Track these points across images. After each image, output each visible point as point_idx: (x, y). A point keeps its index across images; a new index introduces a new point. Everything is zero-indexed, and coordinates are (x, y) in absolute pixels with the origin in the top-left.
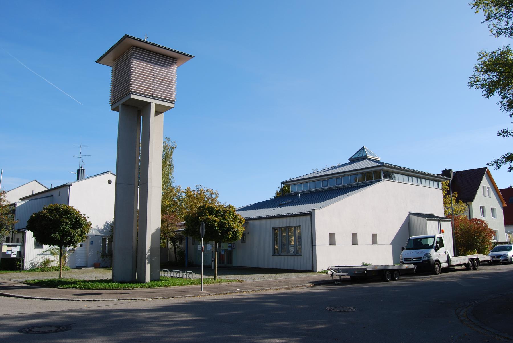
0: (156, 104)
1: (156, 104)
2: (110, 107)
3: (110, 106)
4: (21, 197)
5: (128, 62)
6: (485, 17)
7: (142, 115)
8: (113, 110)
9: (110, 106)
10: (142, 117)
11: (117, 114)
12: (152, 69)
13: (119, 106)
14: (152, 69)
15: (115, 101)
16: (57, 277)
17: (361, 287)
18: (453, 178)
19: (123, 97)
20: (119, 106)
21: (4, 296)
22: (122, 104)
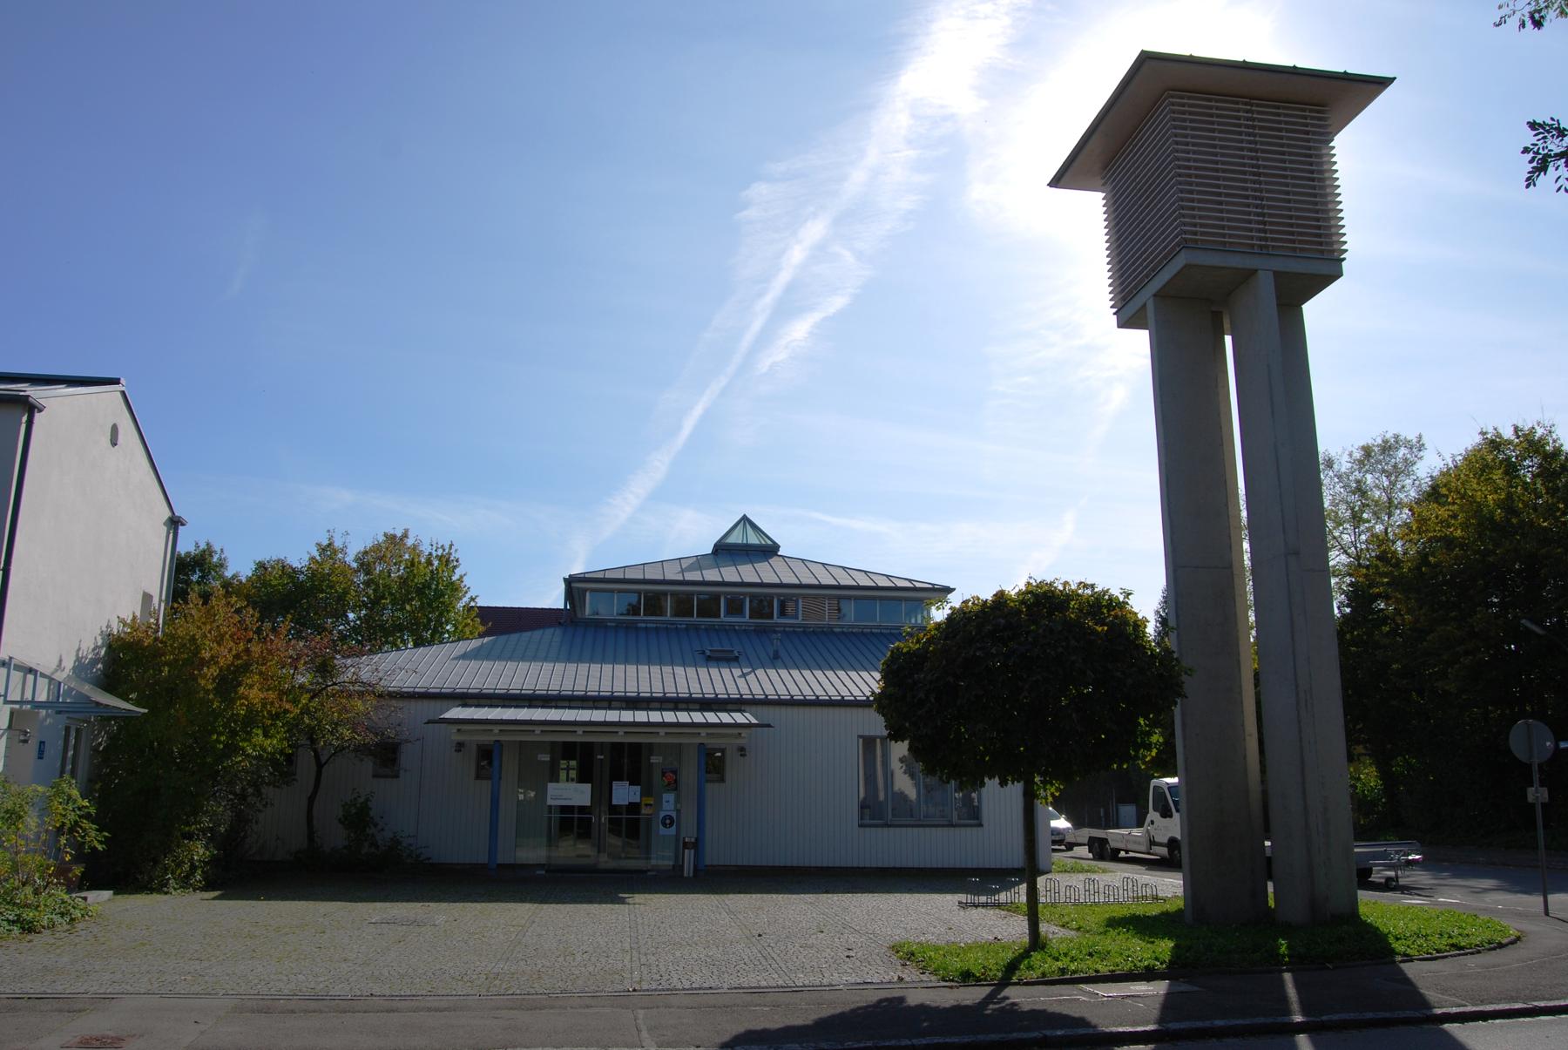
0: (1277, 274)
1: (1277, 274)
2: (1115, 316)
3: (1114, 314)
4: (1395, 81)
5: (1123, 226)
6: (1130, 597)
7: (1227, 325)
8: (1123, 324)
9: (1114, 314)
10: (1228, 340)
11: (1140, 340)
12: (1246, 161)
13: (1145, 305)
14: (1246, 161)
15: (1130, 291)
16: (602, 577)
17: (1114, 1029)
18: (862, 795)
19: (1154, 271)
20: (1145, 305)
21: (765, 1031)
22: (1155, 295)
